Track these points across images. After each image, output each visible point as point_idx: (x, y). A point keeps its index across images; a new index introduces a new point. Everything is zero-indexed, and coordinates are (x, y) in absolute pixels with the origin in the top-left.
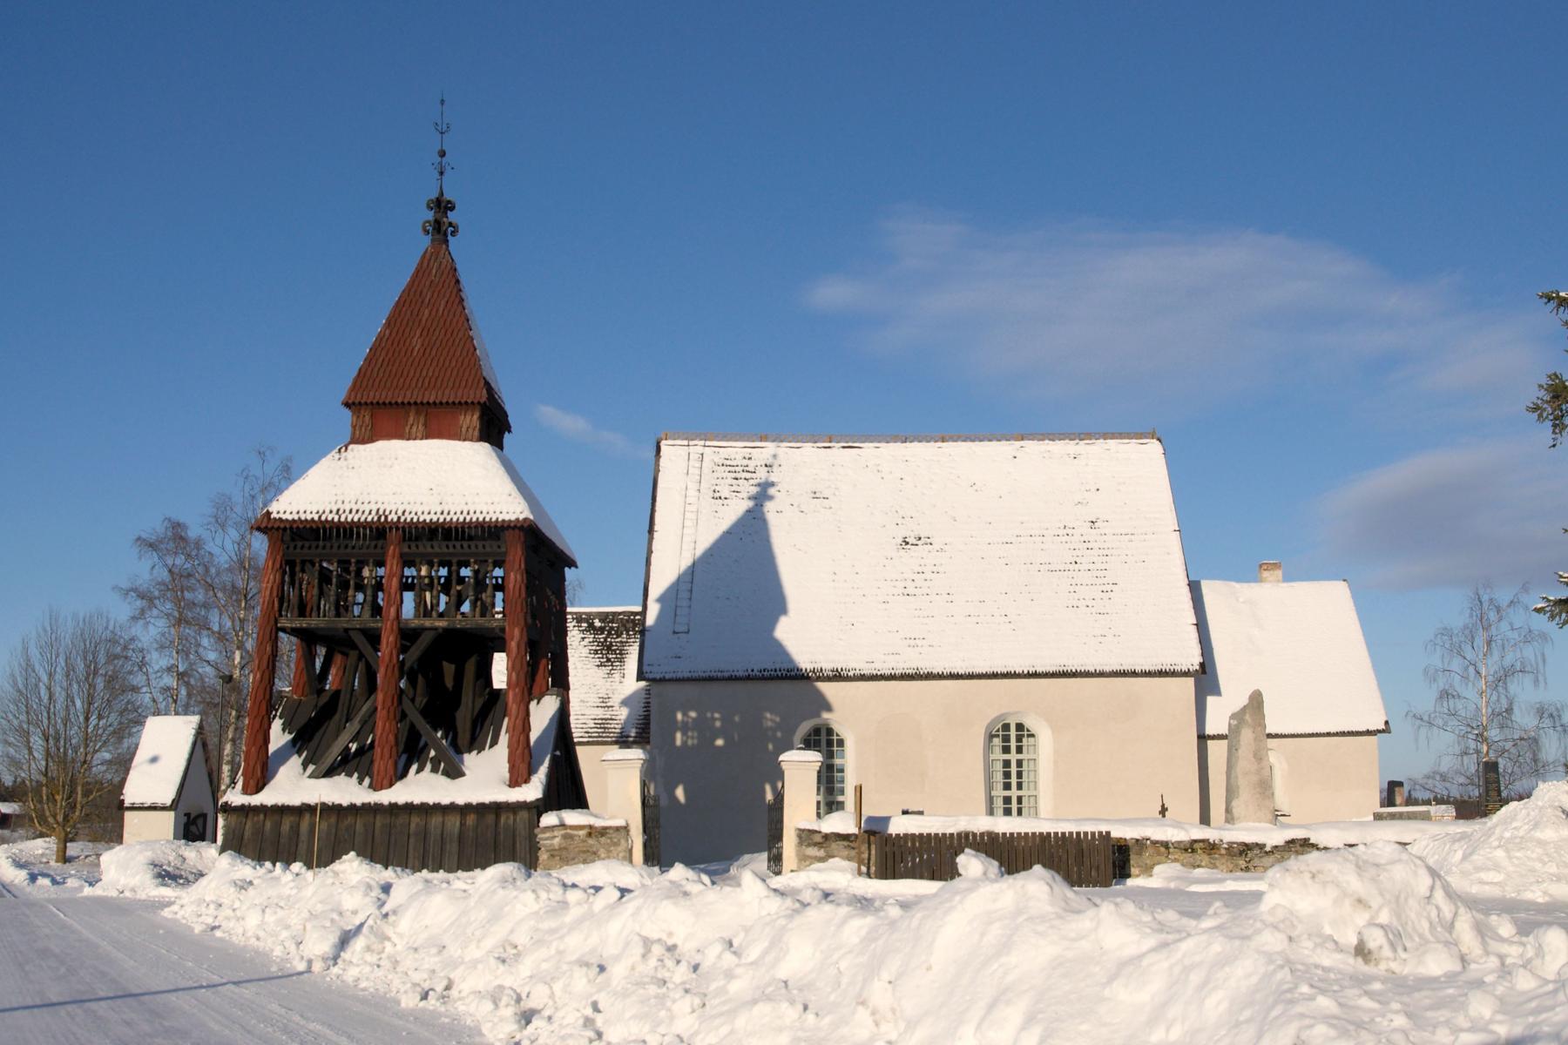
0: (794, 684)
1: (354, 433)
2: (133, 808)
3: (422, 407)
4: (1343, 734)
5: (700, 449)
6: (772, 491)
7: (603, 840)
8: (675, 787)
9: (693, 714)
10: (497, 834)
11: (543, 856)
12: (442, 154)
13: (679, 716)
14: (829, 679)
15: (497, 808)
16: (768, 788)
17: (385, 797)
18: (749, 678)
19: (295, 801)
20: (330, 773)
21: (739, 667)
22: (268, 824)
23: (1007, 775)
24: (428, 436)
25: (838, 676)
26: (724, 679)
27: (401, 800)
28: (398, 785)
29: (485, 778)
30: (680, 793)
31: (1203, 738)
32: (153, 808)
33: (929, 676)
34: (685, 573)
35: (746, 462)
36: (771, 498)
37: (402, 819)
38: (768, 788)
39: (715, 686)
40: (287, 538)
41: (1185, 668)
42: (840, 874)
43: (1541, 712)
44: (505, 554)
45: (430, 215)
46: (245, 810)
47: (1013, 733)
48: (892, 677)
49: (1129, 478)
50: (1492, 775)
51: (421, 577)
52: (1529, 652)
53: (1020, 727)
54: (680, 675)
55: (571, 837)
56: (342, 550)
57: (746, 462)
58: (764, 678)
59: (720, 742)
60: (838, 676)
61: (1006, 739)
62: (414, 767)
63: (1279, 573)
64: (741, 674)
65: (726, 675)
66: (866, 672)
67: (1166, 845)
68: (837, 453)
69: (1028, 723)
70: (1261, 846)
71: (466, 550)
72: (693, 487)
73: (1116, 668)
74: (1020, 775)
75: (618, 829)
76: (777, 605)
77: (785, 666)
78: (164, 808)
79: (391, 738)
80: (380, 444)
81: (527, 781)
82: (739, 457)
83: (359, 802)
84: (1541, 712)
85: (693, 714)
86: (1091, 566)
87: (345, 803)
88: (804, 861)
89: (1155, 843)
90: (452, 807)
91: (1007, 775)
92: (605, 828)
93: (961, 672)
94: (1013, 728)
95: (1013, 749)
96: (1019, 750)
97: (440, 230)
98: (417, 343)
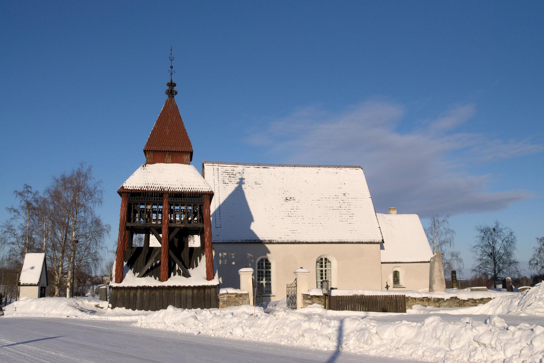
0: (259, 244)
1: (147, 161)
2: (24, 285)
3: (171, 152)
4: (420, 262)
5: (217, 167)
7: (241, 298)
9: (225, 254)
10: (204, 296)
11: (221, 304)
12: (172, 67)
13: (220, 255)
14: (268, 243)
15: (204, 287)
17: (166, 284)
18: (242, 243)
19: (135, 285)
20: (144, 276)
21: (239, 239)
22: (126, 294)
23: (322, 275)
24: (173, 162)
25: (271, 242)
26: (234, 243)
27: (172, 285)
28: (169, 280)
29: (198, 277)
32: (31, 285)
33: (299, 243)
34: (218, 209)
35: (232, 172)
36: (244, 183)
37: (172, 291)
39: (230, 245)
40: (129, 195)
42: (317, 309)
43: (452, 255)
44: (203, 203)
45: (168, 88)
46: (117, 288)
47: (324, 261)
48: (288, 243)
49: (353, 181)
50: (454, 275)
51: (147, 209)
52: (448, 236)
53: (326, 259)
54: (219, 241)
55: (230, 297)
56: (136, 200)
57: (232, 172)
58: (247, 243)
59: (234, 263)
60: (271, 242)
61: (322, 263)
62: (172, 274)
63: (396, 211)
64: (239, 241)
67: (415, 299)
68: (261, 169)
69: (328, 258)
70: (443, 299)
71: (178, 201)
74: (326, 275)
75: (246, 294)
76: (250, 219)
78: (35, 285)
79: (167, 264)
80: (157, 164)
81: (213, 278)
82: (230, 170)
83: (157, 286)
84: (452, 255)
85: (225, 254)
87: (152, 286)
88: (305, 305)
89: (412, 298)
90: (189, 287)
91: (322, 275)
92: (242, 294)
93: (309, 241)
94: (324, 260)
95: (324, 266)
97: (171, 93)
98: (168, 131)
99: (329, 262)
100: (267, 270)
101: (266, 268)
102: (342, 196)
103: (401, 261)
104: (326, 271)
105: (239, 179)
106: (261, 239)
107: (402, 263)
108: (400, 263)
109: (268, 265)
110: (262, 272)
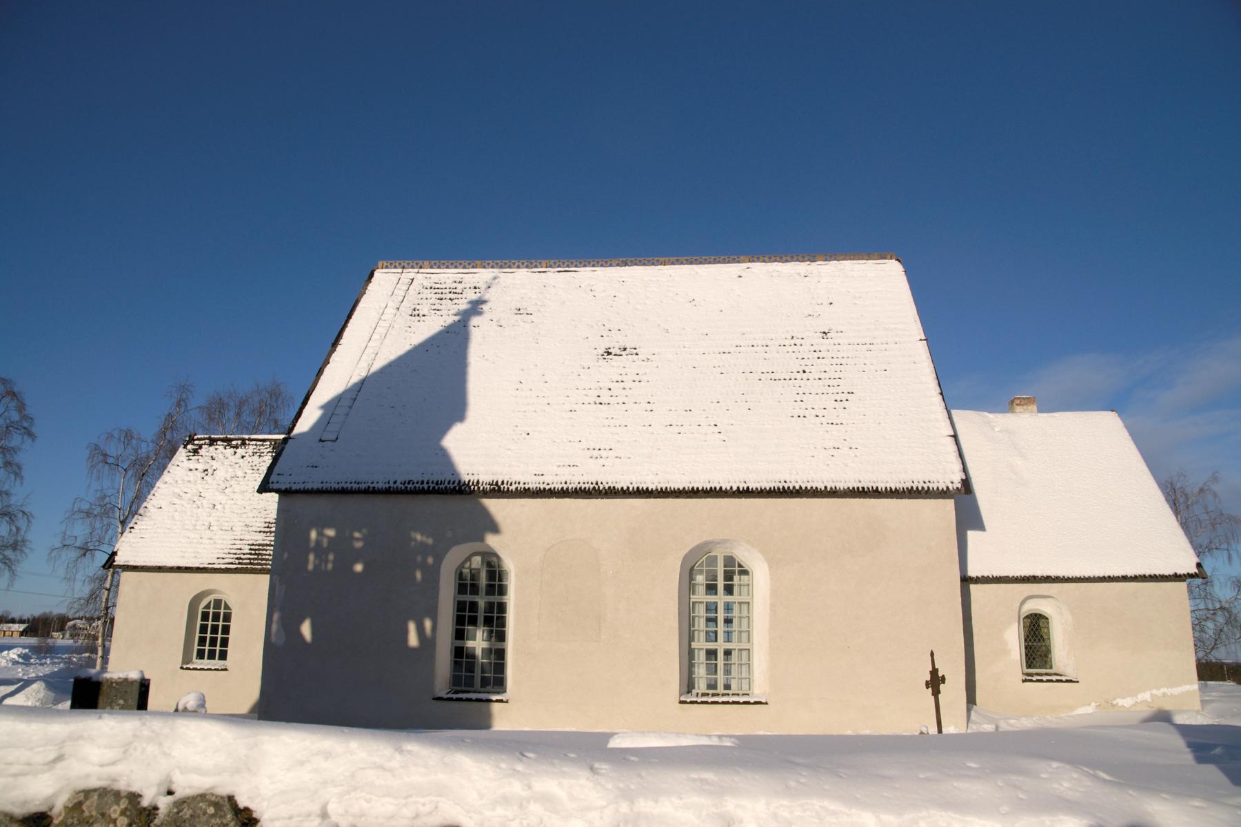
0: (460, 499)
4: (1135, 579)
6: (485, 307)
8: (301, 621)
9: (331, 533)
13: (313, 535)
16: (412, 627)
18: (388, 492)
23: (712, 620)
25: (498, 491)
30: (306, 629)
31: (966, 581)
34: (356, 384)
38: (412, 627)
41: (942, 486)
48: (563, 493)
49: (869, 298)
53: (729, 561)
54: (309, 486)
64: (381, 486)
65: (363, 486)
66: (532, 486)
72: (392, 305)
73: (852, 484)
76: (456, 410)
77: (449, 477)
85: (331, 533)
86: (823, 375)
91: (712, 620)
94: (721, 563)
96: (729, 590)
99: (745, 572)
100: (492, 599)
101: (491, 589)
102: (817, 340)
103: (1053, 572)
104: (728, 607)
105: (471, 302)
106: (465, 478)
107: (1058, 580)
108: (1047, 579)
109: (496, 580)
110: (474, 606)
